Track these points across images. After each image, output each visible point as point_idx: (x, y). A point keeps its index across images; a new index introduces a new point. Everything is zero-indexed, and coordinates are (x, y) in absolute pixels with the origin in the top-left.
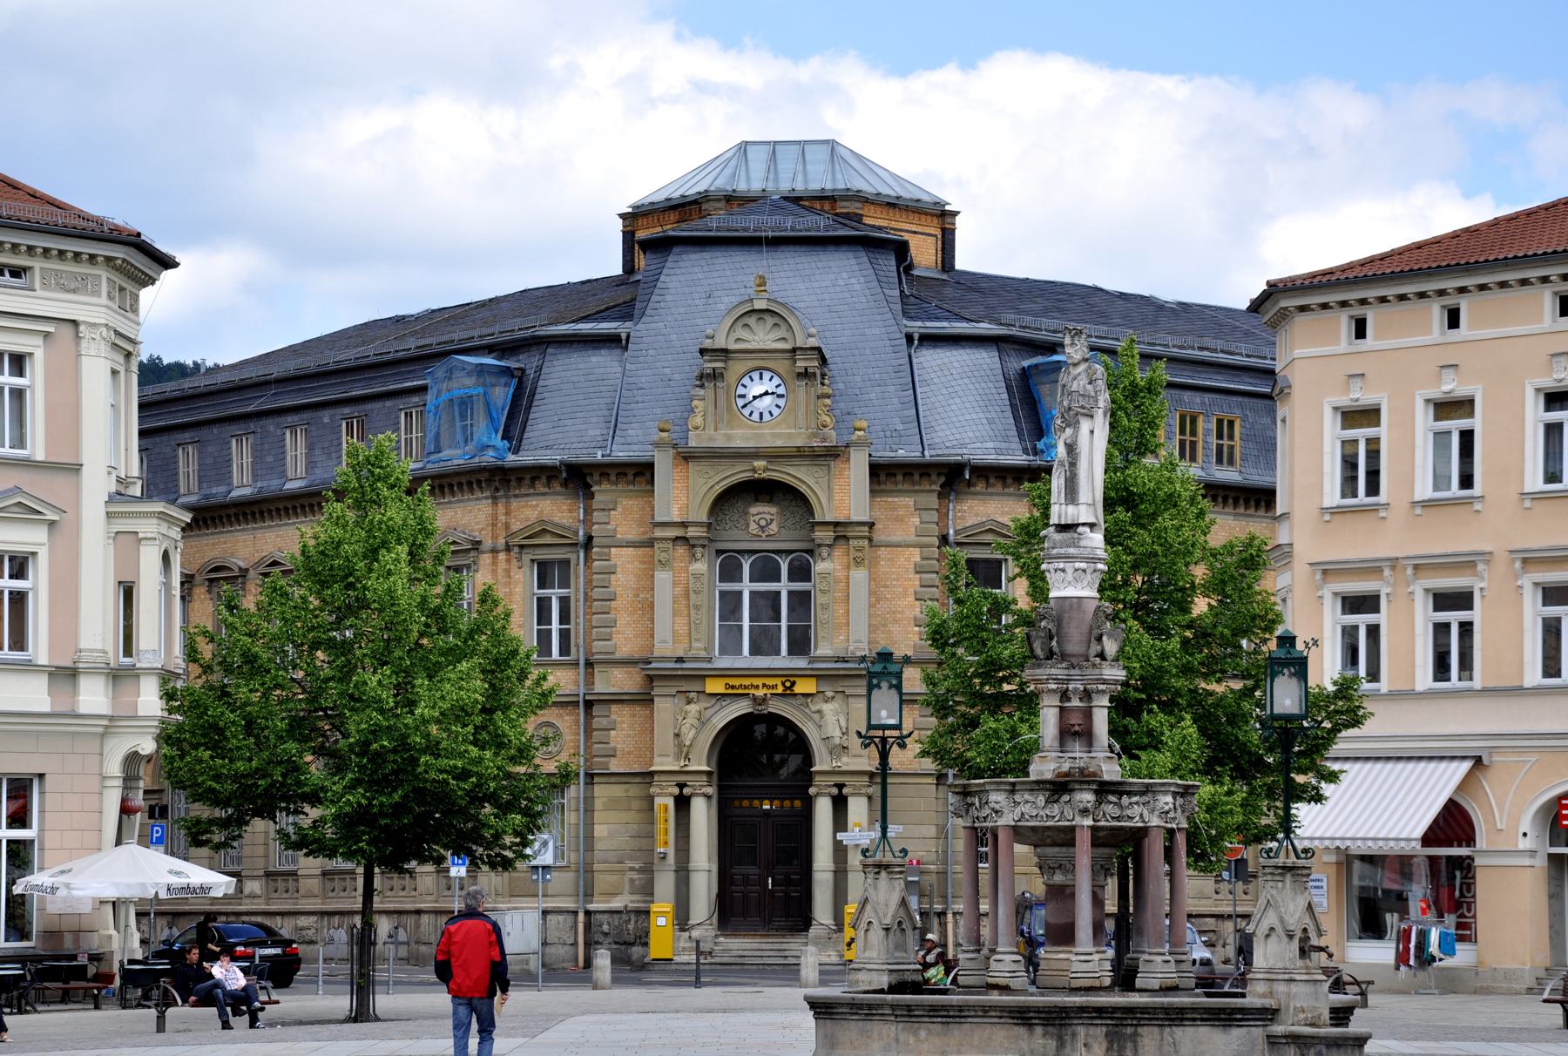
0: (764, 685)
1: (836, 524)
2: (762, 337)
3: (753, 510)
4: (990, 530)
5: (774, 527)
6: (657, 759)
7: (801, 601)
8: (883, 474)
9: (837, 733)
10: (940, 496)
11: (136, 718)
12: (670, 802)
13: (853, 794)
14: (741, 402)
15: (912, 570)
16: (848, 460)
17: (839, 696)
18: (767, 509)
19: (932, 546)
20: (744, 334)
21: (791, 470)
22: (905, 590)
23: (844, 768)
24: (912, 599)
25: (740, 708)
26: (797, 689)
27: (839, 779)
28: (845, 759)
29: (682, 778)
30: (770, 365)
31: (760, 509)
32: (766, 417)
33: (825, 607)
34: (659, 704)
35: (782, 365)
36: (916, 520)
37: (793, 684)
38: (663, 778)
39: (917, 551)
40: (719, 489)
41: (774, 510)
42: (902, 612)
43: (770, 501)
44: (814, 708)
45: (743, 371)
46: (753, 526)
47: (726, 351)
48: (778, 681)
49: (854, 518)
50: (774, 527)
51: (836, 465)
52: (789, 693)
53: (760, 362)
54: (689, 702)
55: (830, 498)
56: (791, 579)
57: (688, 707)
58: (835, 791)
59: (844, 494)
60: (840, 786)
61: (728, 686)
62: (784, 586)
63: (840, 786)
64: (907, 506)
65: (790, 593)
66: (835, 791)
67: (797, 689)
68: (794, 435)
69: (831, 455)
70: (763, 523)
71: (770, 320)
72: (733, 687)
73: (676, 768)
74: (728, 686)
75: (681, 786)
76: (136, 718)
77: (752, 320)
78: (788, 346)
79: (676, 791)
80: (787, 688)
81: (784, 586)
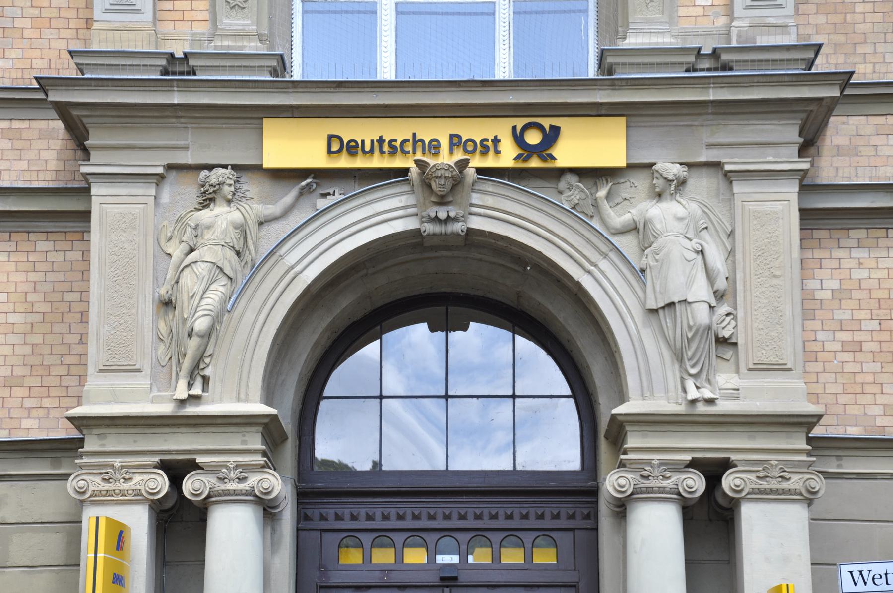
0: (455, 141)
6: (95, 382)
9: (700, 291)
12: (138, 522)
13: (761, 495)
17: (702, 185)
23: (725, 406)
25: (386, 216)
26: (566, 154)
28: (725, 379)
29: (178, 444)
34: (105, 202)
37: (552, 136)
44: (618, 218)
48: (501, 129)
52: (536, 173)
54: (207, 201)
57: (206, 215)
60: (714, 470)
63: (714, 470)
67: (566, 154)
72: (352, 148)
73: (166, 408)
75: (176, 470)
79: (161, 483)
80: (527, 151)
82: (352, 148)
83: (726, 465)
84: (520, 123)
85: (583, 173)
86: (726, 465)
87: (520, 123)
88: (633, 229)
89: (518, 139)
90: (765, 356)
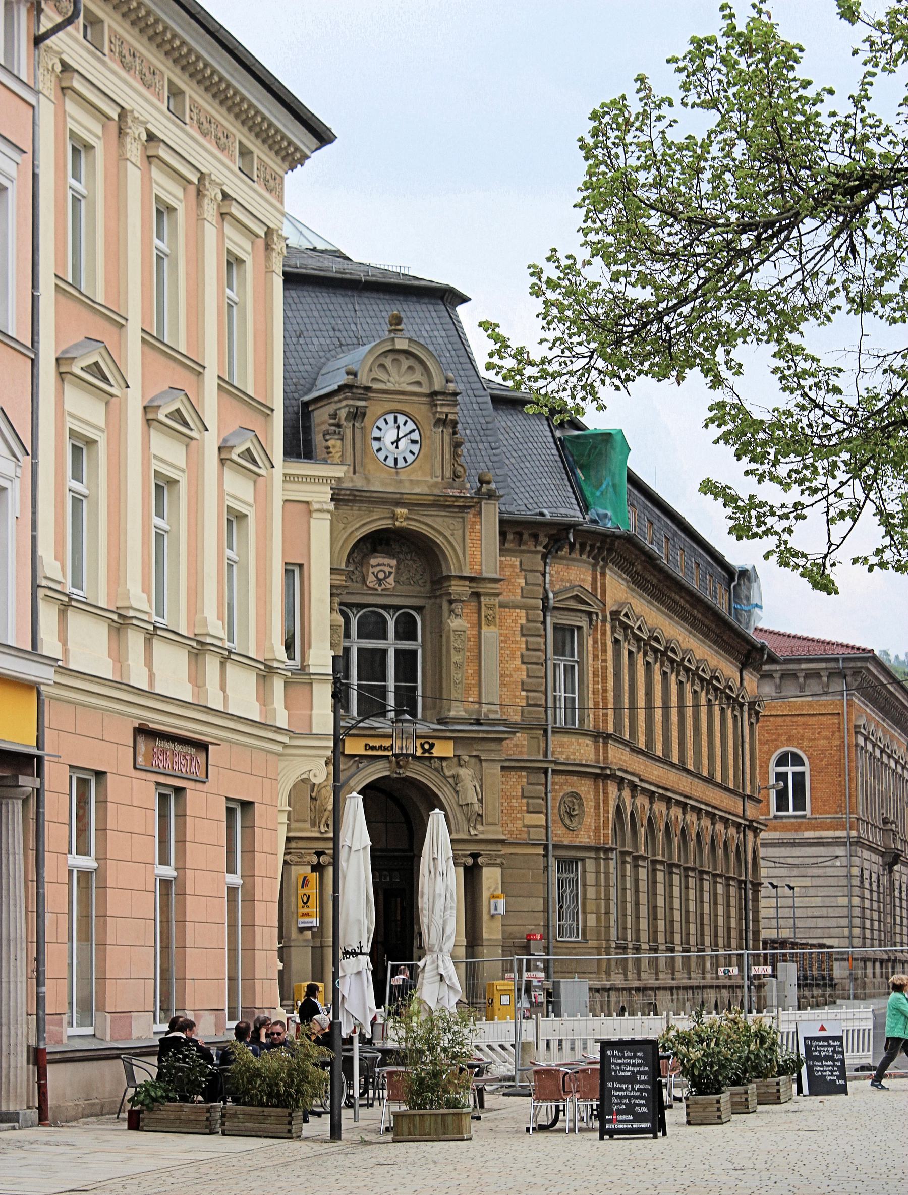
1: (471, 579)
2: (399, 379)
3: (373, 562)
4: (576, 598)
5: (391, 579)
7: (406, 660)
8: (515, 531)
10: (544, 557)
11: (311, 735)
13: (489, 865)
14: (376, 445)
15: (518, 633)
16: (480, 513)
18: (387, 561)
19: (537, 608)
20: (382, 376)
21: (428, 520)
22: (513, 653)
23: (481, 837)
24: (518, 662)
26: (436, 752)
27: (474, 848)
30: (407, 409)
31: (380, 561)
32: (401, 463)
33: (458, 666)
35: (421, 410)
36: (522, 581)
37: (432, 746)
38: (301, 844)
39: (523, 613)
40: (359, 535)
41: (394, 563)
42: (511, 676)
43: (392, 556)
45: (379, 413)
46: (371, 578)
47: (368, 389)
49: (485, 575)
50: (391, 579)
51: (470, 516)
52: (427, 759)
53: (398, 404)
55: (464, 555)
56: (398, 637)
58: (470, 861)
59: (475, 548)
60: (475, 856)
61: (368, 747)
62: (391, 645)
64: (513, 566)
65: (397, 651)
66: (470, 861)
67: (436, 752)
68: (422, 481)
69: (463, 508)
70: (381, 575)
71: (406, 363)
72: (373, 748)
73: (317, 835)
74: (368, 747)
76: (311, 735)
77: (388, 362)
78: (425, 390)
80: (425, 751)
81: (391, 645)
82: (373, 748)
83: (478, 855)
84: (423, 741)
85: (442, 759)
86: (478, 855)
87: (423, 741)
88: (453, 776)
89: (422, 745)
90: (490, 820)
